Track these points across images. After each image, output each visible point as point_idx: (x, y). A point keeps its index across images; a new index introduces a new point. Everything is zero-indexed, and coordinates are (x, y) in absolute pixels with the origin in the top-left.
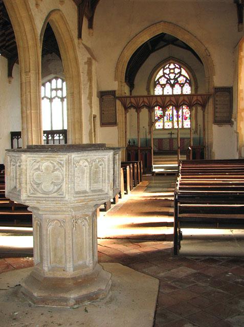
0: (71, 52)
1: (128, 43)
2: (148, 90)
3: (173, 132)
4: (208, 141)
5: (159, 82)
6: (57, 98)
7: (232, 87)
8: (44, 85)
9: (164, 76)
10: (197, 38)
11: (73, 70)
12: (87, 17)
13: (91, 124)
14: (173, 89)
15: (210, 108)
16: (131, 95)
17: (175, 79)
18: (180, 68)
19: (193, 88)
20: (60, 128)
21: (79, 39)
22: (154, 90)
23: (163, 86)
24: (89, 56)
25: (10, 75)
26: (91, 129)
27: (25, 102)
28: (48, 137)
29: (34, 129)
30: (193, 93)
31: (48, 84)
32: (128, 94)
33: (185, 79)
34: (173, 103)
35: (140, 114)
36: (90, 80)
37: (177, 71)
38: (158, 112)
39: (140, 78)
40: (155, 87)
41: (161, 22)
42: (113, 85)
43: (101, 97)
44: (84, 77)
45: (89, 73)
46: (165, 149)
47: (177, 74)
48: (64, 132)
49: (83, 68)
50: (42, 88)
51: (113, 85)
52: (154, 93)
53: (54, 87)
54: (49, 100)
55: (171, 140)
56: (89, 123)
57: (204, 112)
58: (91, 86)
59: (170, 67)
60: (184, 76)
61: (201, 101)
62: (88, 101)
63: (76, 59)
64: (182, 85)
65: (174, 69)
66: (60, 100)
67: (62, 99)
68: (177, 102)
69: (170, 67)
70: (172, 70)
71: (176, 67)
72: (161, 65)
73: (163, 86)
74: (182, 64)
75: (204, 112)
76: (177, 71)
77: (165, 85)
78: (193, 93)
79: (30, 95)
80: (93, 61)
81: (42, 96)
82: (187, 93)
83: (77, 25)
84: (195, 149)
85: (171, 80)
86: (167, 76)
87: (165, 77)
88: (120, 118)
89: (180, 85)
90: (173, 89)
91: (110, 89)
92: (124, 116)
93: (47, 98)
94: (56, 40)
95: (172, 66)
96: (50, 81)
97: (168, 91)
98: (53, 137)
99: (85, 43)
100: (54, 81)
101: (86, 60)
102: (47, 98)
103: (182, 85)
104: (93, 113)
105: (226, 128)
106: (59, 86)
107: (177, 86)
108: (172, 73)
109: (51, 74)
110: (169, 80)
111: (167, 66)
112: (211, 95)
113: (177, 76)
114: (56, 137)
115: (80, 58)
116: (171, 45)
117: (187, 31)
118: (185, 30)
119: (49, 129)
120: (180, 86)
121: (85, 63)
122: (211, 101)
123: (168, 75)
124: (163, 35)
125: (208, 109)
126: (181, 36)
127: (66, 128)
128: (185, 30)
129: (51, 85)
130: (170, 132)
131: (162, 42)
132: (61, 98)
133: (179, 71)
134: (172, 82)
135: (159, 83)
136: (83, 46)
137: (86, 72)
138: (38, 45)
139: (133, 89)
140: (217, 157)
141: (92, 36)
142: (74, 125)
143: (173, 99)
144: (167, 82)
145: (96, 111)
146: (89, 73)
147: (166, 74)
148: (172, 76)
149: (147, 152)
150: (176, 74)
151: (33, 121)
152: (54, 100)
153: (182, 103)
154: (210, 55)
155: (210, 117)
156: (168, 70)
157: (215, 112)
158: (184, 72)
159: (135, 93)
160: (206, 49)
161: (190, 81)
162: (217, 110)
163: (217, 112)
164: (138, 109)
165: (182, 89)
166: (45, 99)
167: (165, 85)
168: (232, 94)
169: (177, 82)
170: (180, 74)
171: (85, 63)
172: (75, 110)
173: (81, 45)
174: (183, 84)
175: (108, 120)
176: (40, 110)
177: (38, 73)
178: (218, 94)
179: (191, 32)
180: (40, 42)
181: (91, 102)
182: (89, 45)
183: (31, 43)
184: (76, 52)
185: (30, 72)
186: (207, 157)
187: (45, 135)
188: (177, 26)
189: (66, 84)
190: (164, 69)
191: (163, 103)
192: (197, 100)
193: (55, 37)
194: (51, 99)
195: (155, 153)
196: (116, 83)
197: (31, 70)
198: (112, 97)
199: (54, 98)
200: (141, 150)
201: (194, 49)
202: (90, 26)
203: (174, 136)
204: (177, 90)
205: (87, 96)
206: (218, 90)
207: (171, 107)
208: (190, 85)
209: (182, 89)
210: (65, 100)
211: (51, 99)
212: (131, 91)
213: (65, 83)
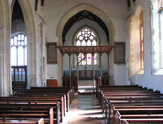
0: (30, 18)
1: (65, 15)
2: (73, 44)
3: (87, 67)
4: (111, 74)
5: (79, 39)
6: (21, 46)
7: (125, 42)
8: (13, 38)
9: (81, 35)
10: (105, 14)
11: (32, 29)
13: (41, 62)
14: (86, 43)
15: (112, 54)
16: (63, 45)
18: (91, 31)
19: (98, 42)
21: (35, 11)
22: (76, 43)
23: (81, 41)
24: (42, 21)
26: (42, 66)
27: (33, 64)
28: (14, 71)
29: (5, 66)
30: (98, 45)
31: (16, 38)
32: (62, 45)
33: (93, 37)
34: (82, 51)
35: (71, 57)
36: (42, 35)
37: (89, 33)
38: (82, 55)
40: (77, 41)
41: (84, 3)
42: (56, 39)
43: (48, 46)
44: (38, 34)
45: (41, 31)
46: (83, 77)
47: (89, 34)
48: (25, 67)
49: (37, 28)
50: (12, 40)
51: (56, 39)
52: (76, 45)
53: (19, 39)
54: (16, 47)
56: (40, 62)
57: (108, 56)
58: (42, 39)
59: (85, 31)
60: (93, 36)
61: (107, 50)
62: (40, 49)
63: (34, 23)
64: (92, 41)
65: (87, 32)
66: (22, 47)
67: (24, 47)
68: (92, 50)
69: (85, 31)
70: (86, 32)
71: (88, 31)
72: (80, 29)
73: (81, 41)
74: (92, 29)
75: (108, 56)
76: (89, 33)
77: (82, 40)
78: (98, 45)
79: (3, 43)
80: (44, 24)
81: (12, 44)
82: (94, 45)
83: (35, 2)
84: (103, 78)
85: (86, 38)
86: (83, 36)
87: (82, 36)
89: (91, 40)
90: (86, 43)
91: (53, 41)
92: (61, 58)
93: (15, 46)
94: (21, 11)
95: (86, 30)
96: (17, 36)
97: (84, 44)
98: (18, 70)
99: (39, 14)
100: (19, 36)
101: (39, 24)
102: (15, 46)
103: (92, 41)
104: (43, 56)
105: (122, 66)
106: (22, 39)
107: (89, 41)
108: (86, 34)
109: (18, 31)
110: (84, 37)
111: (84, 30)
112: (113, 47)
113: (89, 36)
114: (20, 70)
115: (36, 22)
117: (99, 9)
118: (98, 9)
119: (16, 65)
120: (91, 41)
121: (39, 25)
122: (113, 50)
123: (84, 35)
125: (111, 54)
126: (95, 12)
127: (26, 65)
128: (98, 9)
129: (17, 38)
130: (85, 67)
131: (81, 17)
132: (23, 46)
133: (90, 33)
134: (86, 39)
135: (79, 39)
136: (38, 15)
137: (39, 31)
138: (9, 10)
139: (64, 42)
140: (117, 83)
141: (43, 10)
142: (31, 64)
143: (91, 49)
144: (83, 39)
145: (45, 55)
146: (41, 31)
147: (83, 34)
148: (86, 36)
149: (75, 80)
150: (88, 35)
151: (4, 61)
152: (19, 47)
153: (104, 51)
154: (112, 24)
156: (84, 32)
157: (115, 57)
158: (93, 34)
159: (66, 44)
160: (110, 20)
161: (96, 38)
162: (116, 55)
163: (116, 57)
165: (92, 43)
166: (14, 46)
167: (82, 40)
168: (125, 47)
169: (89, 39)
170: (91, 35)
171: (39, 25)
172: (32, 54)
173: (37, 15)
174: (92, 40)
175: (51, 60)
176: (9, 53)
177: (9, 29)
178: (116, 46)
179: (101, 10)
180: (11, 10)
181: (42, 49)
182: (41, 16)
183: (4, 9)
184: (33, 17)
185: (3, 28)
186: (111, 84)
187: (13, 69)
188: (93, 6)
189: (27, 37)
190: (82, 32)
191: (93, 51)
192: (105, 49)
193: (21, 9)
194: (17, 47)
195: (79, 79)
197: (4, 27)
198: (54, 46)
199: (19, 46)
200: (71, 79)
201: (102, 20)
202: (42, 4)
203: (87, 69)
204: (89, 43)
205: (40, 45)
206: (117, 44)
207: (81, 53)
208: (96, 41)
209: (92, 43)
210: (26, 47)
211: (17, 47)
212: (63, 43)
213: (26, 37)
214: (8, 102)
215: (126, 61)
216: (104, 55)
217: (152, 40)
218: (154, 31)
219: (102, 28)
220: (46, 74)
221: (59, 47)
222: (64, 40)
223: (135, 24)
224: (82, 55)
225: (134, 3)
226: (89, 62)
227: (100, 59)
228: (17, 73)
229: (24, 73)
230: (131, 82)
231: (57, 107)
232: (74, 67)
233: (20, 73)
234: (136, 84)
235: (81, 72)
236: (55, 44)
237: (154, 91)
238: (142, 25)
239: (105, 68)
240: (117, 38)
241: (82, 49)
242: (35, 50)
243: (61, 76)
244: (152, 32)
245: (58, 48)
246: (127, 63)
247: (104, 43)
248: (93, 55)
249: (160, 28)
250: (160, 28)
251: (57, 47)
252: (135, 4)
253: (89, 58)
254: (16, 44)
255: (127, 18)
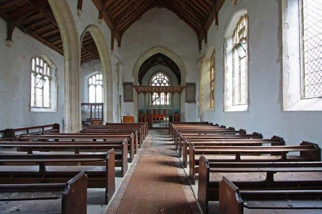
2: (149, 84)
12: (116, 38)
15: (183, 94)
17: (162, 81)
20: (101, 102)
25: (9, 38)
31: (94, 77)
36: (118, 75)
37: (163, 77)
39: (144, 79)
42: (132, 79)
45: (118, 71)
48: (102, 104)
50: (90, 79)
51: (132, 79)
55: (159, 110)
68: (165, 90)
76: (163, 77)
81: (90, 83)
85: (160, 79)
88: (135, 98)
96: (95, 75)
100: (97, 75)
110: (159, 81)
116: (160, 65)
119: (94, 102)
122: (184, 90)
124: (159, 54)
134: (160, 82)
145: (121, 93)
148: (160, 80)
155: (183, 98)
158: (166, 78)
164: (145, 93)
170: (164, 79)
186: (182, 121)
194: (96, 86)
196: (133, 78)
202: (119, 45)
203: (161, 108)
204: (162, 85)
206: (188, 84)
211: (96, 86)
214: (73, 140)
215: (197, 100)
216: (176, 94)
217: (225, 77)
218: (227, 69)
219: (175, 71)
220: (123, 112)
221: (135, 87)
222: (140, 81)
223: (206, 66)
224: (155, 95)
225: (216, 27)
226: (163, 103)
227: (172, 99)
228: (93, 110)
229: (101, 111)
230: (201, 119)
231: (123, 146)
232: (149, 106)
233: (97, 111)
234: (205, 121)
235: (94, 58)
236: (131, 84)
237: (227, 127)
238: (213, 66)
239: (176, 108)
240: (188, 79)
241: (157, 88)
242: (112, 87)
243: (137, 113)
244: (225, 70)
245: (136, 88)
246: (198, 102)
247: (175, 84)
248: (166, 95)
249: (233, 66)
250: (233, 66)
251: (133, 86)
252: (206, 46)
253: (163, 99)
254: (94, 83)
255: (200, 60)
